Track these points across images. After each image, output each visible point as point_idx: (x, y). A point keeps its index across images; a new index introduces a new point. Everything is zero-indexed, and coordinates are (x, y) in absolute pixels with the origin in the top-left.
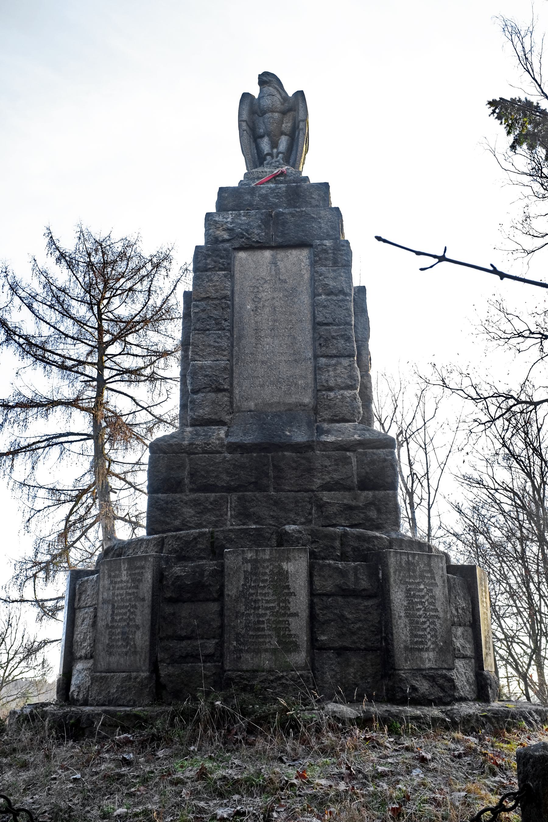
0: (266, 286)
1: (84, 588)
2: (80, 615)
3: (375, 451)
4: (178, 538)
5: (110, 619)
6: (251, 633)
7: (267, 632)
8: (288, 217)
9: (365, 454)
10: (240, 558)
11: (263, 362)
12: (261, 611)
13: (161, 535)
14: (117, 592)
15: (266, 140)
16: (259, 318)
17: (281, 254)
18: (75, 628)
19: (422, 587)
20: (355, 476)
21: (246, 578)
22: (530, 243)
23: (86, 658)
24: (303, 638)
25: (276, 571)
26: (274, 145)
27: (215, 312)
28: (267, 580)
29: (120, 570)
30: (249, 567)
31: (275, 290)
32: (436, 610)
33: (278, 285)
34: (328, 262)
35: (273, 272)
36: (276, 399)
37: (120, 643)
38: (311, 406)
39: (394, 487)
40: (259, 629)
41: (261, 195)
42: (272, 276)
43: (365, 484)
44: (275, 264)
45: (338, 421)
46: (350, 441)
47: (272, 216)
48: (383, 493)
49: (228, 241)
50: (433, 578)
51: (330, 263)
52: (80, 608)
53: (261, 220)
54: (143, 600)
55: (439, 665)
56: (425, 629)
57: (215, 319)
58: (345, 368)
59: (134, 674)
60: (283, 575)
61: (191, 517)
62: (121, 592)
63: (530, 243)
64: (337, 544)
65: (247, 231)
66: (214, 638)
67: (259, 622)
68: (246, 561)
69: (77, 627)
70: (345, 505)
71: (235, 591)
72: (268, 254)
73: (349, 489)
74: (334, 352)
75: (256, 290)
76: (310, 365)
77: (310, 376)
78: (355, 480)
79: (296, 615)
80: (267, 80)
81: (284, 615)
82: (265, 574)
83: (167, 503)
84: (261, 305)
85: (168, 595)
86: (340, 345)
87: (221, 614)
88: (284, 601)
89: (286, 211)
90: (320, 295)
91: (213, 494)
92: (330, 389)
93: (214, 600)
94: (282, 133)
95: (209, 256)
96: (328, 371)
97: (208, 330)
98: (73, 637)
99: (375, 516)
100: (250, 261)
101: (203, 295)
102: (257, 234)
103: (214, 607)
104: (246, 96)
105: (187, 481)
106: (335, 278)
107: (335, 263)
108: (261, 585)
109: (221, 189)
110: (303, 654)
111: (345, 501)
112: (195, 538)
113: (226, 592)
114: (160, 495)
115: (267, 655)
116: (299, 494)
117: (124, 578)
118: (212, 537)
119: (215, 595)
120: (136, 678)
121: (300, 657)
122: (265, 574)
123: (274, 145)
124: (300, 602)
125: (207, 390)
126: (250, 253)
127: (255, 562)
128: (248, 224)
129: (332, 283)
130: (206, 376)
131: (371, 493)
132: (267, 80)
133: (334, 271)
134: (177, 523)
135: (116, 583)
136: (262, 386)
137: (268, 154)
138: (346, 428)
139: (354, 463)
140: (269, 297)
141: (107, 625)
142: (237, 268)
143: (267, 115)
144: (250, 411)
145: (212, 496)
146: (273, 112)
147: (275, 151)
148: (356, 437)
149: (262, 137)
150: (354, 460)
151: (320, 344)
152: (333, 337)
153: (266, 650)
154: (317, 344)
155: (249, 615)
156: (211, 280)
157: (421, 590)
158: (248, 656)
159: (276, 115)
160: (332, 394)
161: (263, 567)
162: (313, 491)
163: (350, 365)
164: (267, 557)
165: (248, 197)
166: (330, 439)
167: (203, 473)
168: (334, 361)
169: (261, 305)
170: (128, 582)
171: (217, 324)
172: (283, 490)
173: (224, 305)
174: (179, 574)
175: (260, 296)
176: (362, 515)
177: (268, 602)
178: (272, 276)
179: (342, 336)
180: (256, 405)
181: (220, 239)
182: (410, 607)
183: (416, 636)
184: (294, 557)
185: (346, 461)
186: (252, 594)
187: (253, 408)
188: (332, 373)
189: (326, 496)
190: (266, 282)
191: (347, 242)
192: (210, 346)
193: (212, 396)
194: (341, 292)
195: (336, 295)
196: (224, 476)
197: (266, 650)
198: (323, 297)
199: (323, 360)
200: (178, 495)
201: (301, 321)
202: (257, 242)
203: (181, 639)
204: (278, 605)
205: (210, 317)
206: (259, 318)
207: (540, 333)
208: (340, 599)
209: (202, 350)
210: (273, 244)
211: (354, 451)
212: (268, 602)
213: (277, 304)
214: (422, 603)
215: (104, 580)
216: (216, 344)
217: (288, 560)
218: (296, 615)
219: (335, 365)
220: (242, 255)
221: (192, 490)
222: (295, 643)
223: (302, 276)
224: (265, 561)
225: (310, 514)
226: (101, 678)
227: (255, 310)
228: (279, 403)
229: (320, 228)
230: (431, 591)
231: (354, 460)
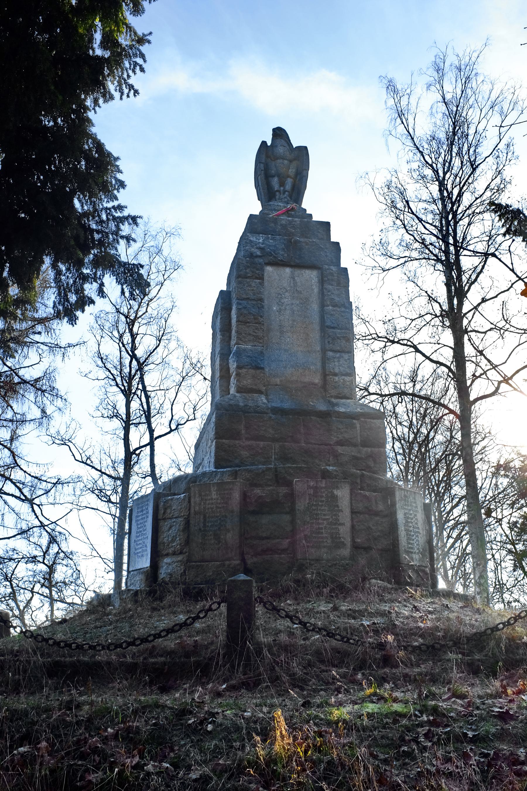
0: (287, 294)
1: (168, 505)
2: (165, 526)
3: (372, 420)
4: (249, 471)
5: (202, 525)
6: (314, 535)
7: (325, 535)
8: (304, 244)
9: (366, 422)
10: (306, 485)
11: (286, 350)
12: (320, 521)
13: (232, 469)
14: (207, 507)
15: (276, 179)
16: (282, 318)
17: (297, 272)
18: (159, 534)
19: (412, 512)
20: (359, 437)
21: (310, 499)
22: (383, 262)
23: (174, 554)
24: (348, 541)
25: (329, 495)
26: (282, 184)
27: (254, 310)
28: (323, 501)
29: (210, 491)
30: (311, 491)
31: (293, 298)
32: (418, 528)
33: (296, 295)
34: (333, 283)
35: (292, 285)
36: (295, 378)
37: (213, 542)
38: (320, 385)
39: (383, 445)
40: (319, 533)
41: (281, 225)
42: (291, 287)
43: (365, 444)
44: (293, 278)
45: (342, 398)
46: (356, 412)
47: (291, 242)
48: (377, 449)
49: (260, 257)
50: (416, 507)
51: (335, 283)
52: (164, 519)
53: (285, 244)
54: (232, 512)
55: (421, 563)
56: (413, 540)
57: (254, 315)
58: (346, 360)
59: (227, 563)
60: (335, 498)
61: (247, 458)
62: (212, 506)
63: (383, 262)
64: (359, 481)
65: (274, 251)
66: (287, 538)
67: (319, 528)
68: (309, 487)
69: (163, 532)
70: (353, 456)
71: (303, 507)
72: (288, 270)
73: (355, 445)
74: (338, 348)
75: (280, 296)
76: (319, 356)
77: (319, 364)
78: (359, 440)
79: (343, 524)
80: (279, 133)
81: (335, 524)
82: (322, 497)
83: (229, 446)
84: (283, 308)
85: (251, 509)
86: (342, 344)
87: (293, 522)
88: (335, 515)
89: (302, 240)
90: (328, 306)
91: (262, 443)
92: (336, 375)
93: (287, 513)
95: (248, 267)
96: (334, 362)
97: (248, 322)
99: (372, 465)
100: (275, 274)
101: (244, 296)
102: (282, 255)
103: (287, 518)
104: (264, 143)
105: (243, 432)
106: (338, 295)
107: (339, 284)
108: (320, 504)
110: (348, 550)
111: (353, 454)
112: (263, 472)
113: (297, 508)
115: (325, 550)
116: (322, 447)
117: (214, 497)
118: (276, 471)
119: (287, 509)
120: (229, 565)
121: (346, 552)
122: (322, 497)
123: (282, 184)
124: (345, 516)
125: (249, 367)
126: (275, 268)
127: (316, 488)
128: (275, 246)
129: (337, 299)
130: (249, 356)
131: (369, 450)
132: (279, 133)
133: (338, 289)
134: (237, 461)
135: (206, 500)
136: (285, 367)
137: (277, 191)
138: (349, 403)
139: (358, 428)
140: (289, 302)
141: (200, 529)
142: (266, 278)
143: (279, 161)
144: (276, 385)
145: (262, 444)
146: (283, 159)
147: (282, 188)
148: (359, 410)
149: (274, 176)
150: (358, 426)
151: (329, 342)
152: (338, 338)
153: (324, 547)
154: (326, 342)
155: (312, 523)
156: (250, 286)
157: (411, 514)
158: (313, 550)
159: (286, 162)
160: (337, 378)
161: (321, 492)
162: (331, 445)
163: (349, 359)
164: (324, 486)
165: (272, 225)
166: (342, 410)
167: (255, 427)
168: (338, 355)
169: (283, 308)
170: (218, 499)
171: (255, 319)
172: (311, 443)
173: (259, 306)
174: (260, 494)
175: (283, 301)
176: (364, 464)
177: (325, 515)
178: (291, 287)
179: (344, 337)
180: (281, 381)
181: (254, 255)
182: (407, 523)
183: (409, 543)
184: (341, 487)
185: (353, 426)
186: (314, 510)
187: (278, 383)
188: (336, 363)
189: (340, 449)
190: (287, 291)
192: (250, 334)
193: (252, 371)
194: (343, 305)
195: (340, 307)
196: (271, 430)
197: (324, 547)
198: (331, 308)
199: (330, 354)
200: (237, 442)
201: (312, 323)
202: (282, 261)
203: (262, 538)
204: (332, 517)
205: (250, 313)
206: (282, 318)
207: (386, 338)
208: (367, 516)
209: (244, 337)
210: (293, 264)
211: (358, 420)
212: (325, 515)
213: (295, 308)
214: (412, 523)
215: (195, 498)
216: (255, 334)
217: (337, 488)
218: (343, 524)
219: (339, 358)
220: (269, 269)
221: (247, 439)
222: (343, 542)
223: (313, 290)
224: (322, 488)
225: (329, 461)
226: (197, 566)
227: (280, 311)
228: (297, 381)
229: (327, 256)
230: (416, 515)
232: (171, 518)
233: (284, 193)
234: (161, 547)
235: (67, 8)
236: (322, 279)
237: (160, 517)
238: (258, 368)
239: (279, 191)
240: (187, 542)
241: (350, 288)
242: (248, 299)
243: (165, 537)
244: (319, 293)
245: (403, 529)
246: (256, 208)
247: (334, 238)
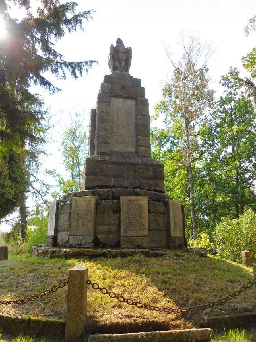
2: (61, 216)
5: (76, 218)
18: (59, 220)
23: (64, 231)
80: (119, 41)
90: (139, 116)
94: (123, 60)
98: (57, 224)
109: (105, 75)
114: (90, 177)
123: (120, 64)
132: (119, 41)
141: (76, 220)
181: (107, 92)
191: (147, 100)
198: (140, 117)
231: (152, 170)
232: (63, 214)
233: (121, 68)
234: (59, 227)
235: (54, 32)
236: (137, 104)
237: (59, 212)
238: (106, 143)
239: (119, 67)
240: (70, 226)
241: (149, 108)
242: (103, 112)
243: (61, 223)
244: (135, 110)
245: (172, 219)
246: (109, 72)
247: (142, 86)
